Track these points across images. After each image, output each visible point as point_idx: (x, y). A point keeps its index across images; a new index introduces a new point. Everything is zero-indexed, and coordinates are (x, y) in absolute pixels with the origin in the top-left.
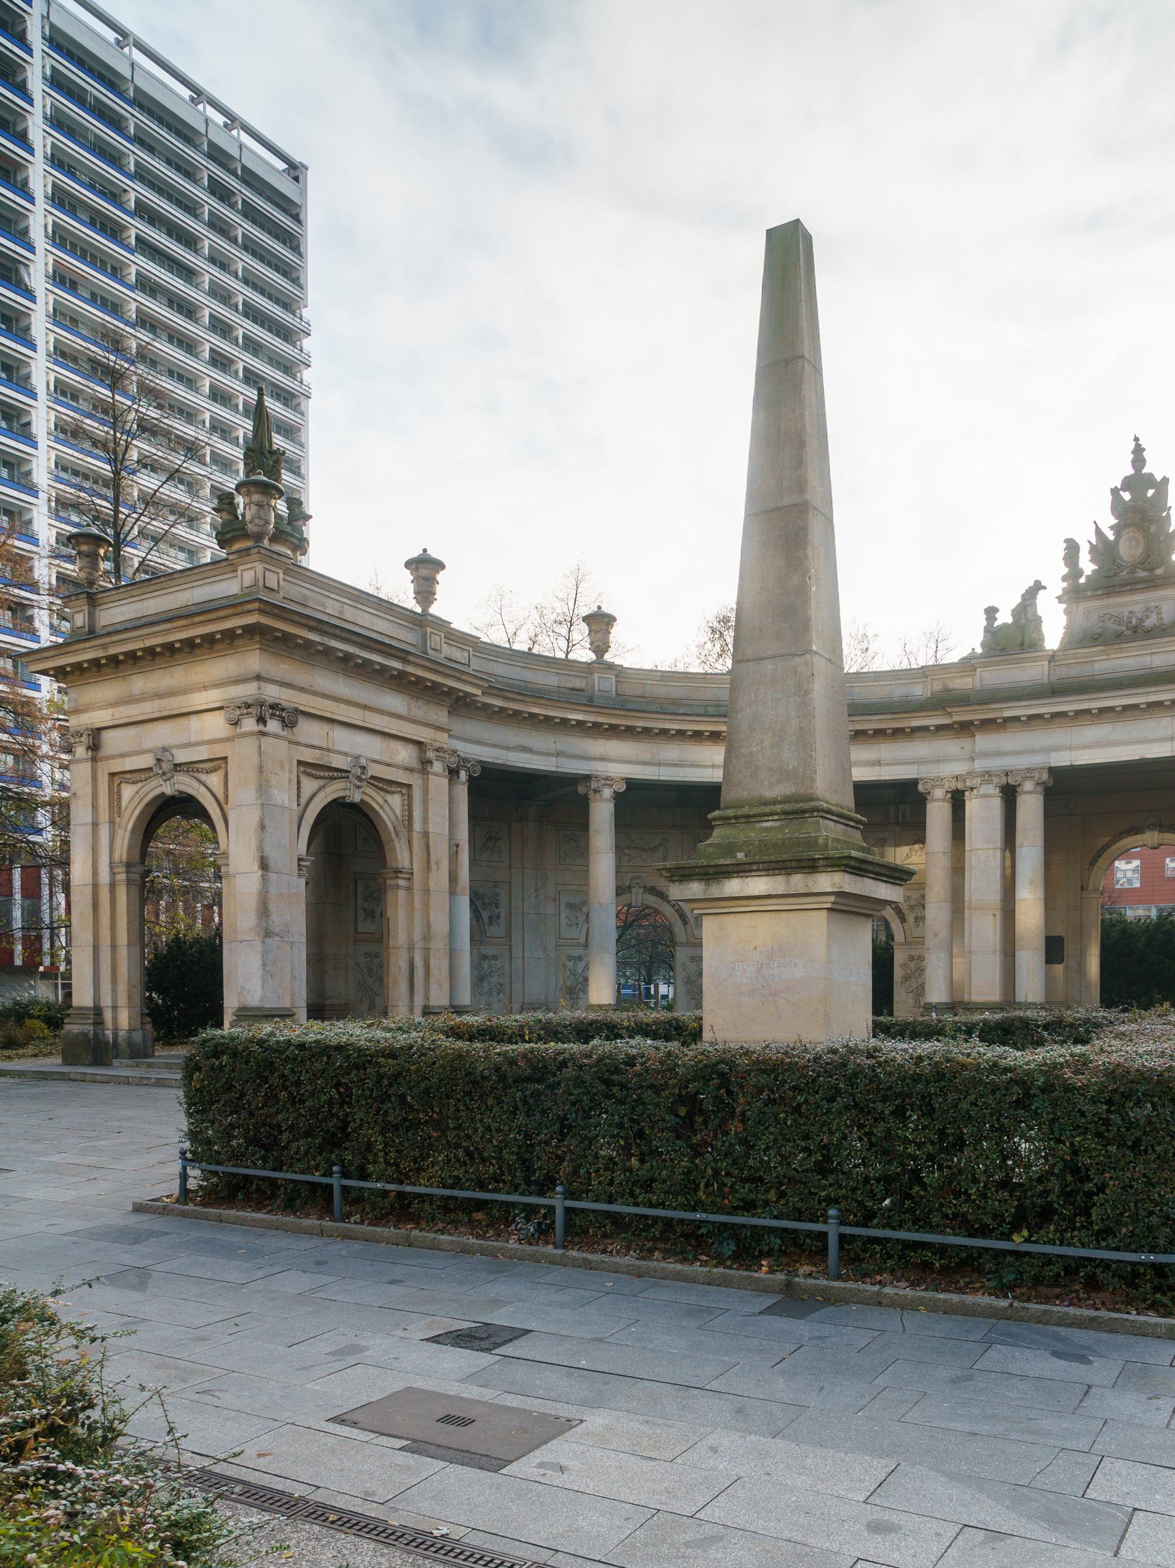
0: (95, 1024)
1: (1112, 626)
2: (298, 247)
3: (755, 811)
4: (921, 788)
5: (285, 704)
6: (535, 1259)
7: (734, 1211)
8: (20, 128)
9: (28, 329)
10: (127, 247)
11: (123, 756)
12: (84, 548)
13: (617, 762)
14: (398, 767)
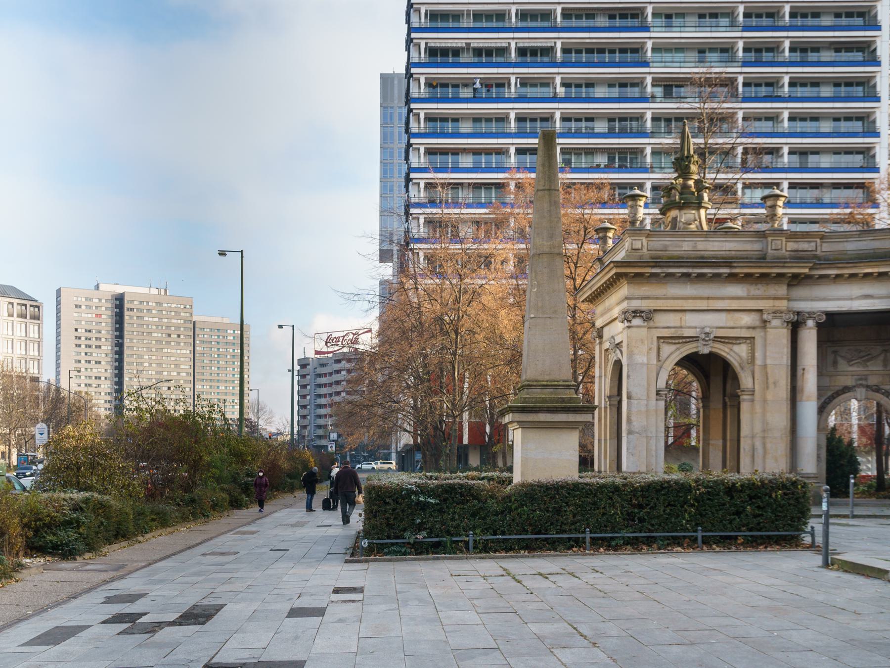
5: (643, 309)
14: (741, 328)
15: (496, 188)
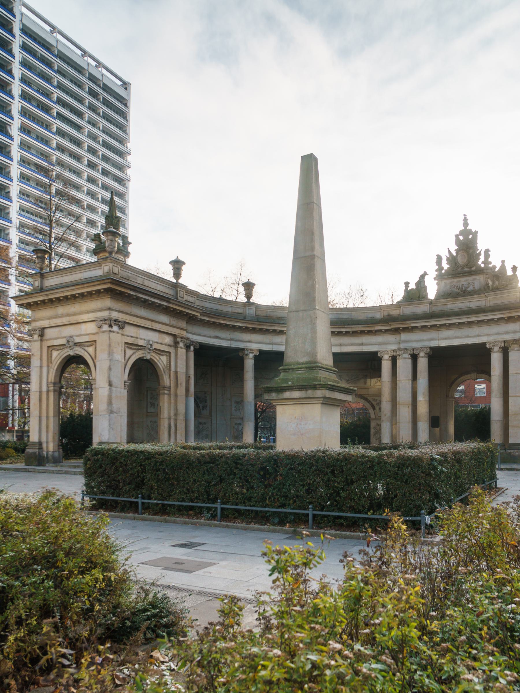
0: (39, 449)
1: (455, 290)
2: (126, 117)
3: (296, 367)
4: (379, 355)
5: (120, 319)
6: (210, 525)
7: (279, 507)
8: (9, 68)
9: (9, 152)
10: (52, 117)
11: (53, 339)
12: (39, 255)
13: (255, 344)
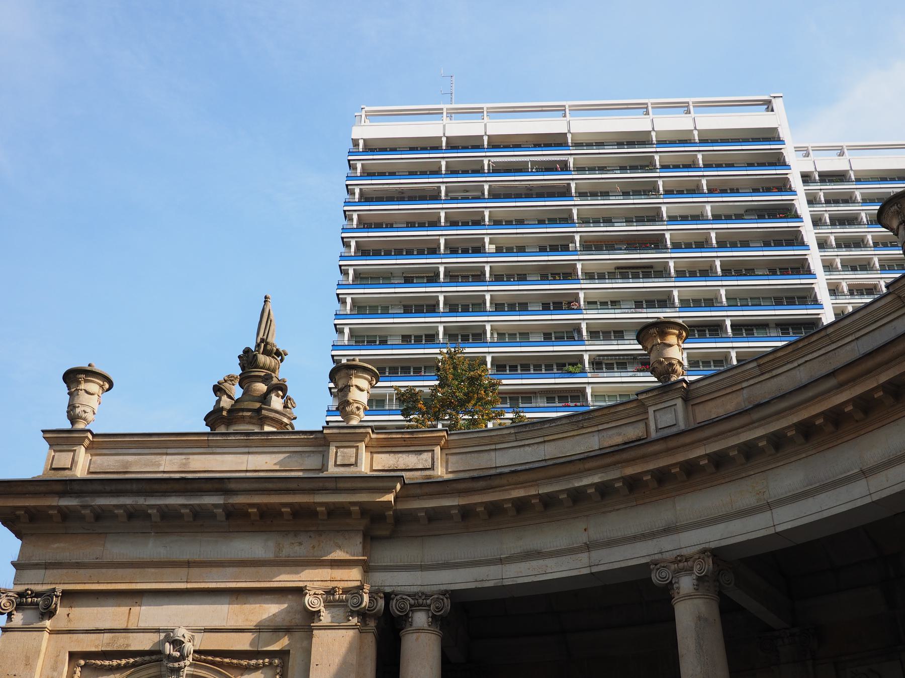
15: (746, 330)
